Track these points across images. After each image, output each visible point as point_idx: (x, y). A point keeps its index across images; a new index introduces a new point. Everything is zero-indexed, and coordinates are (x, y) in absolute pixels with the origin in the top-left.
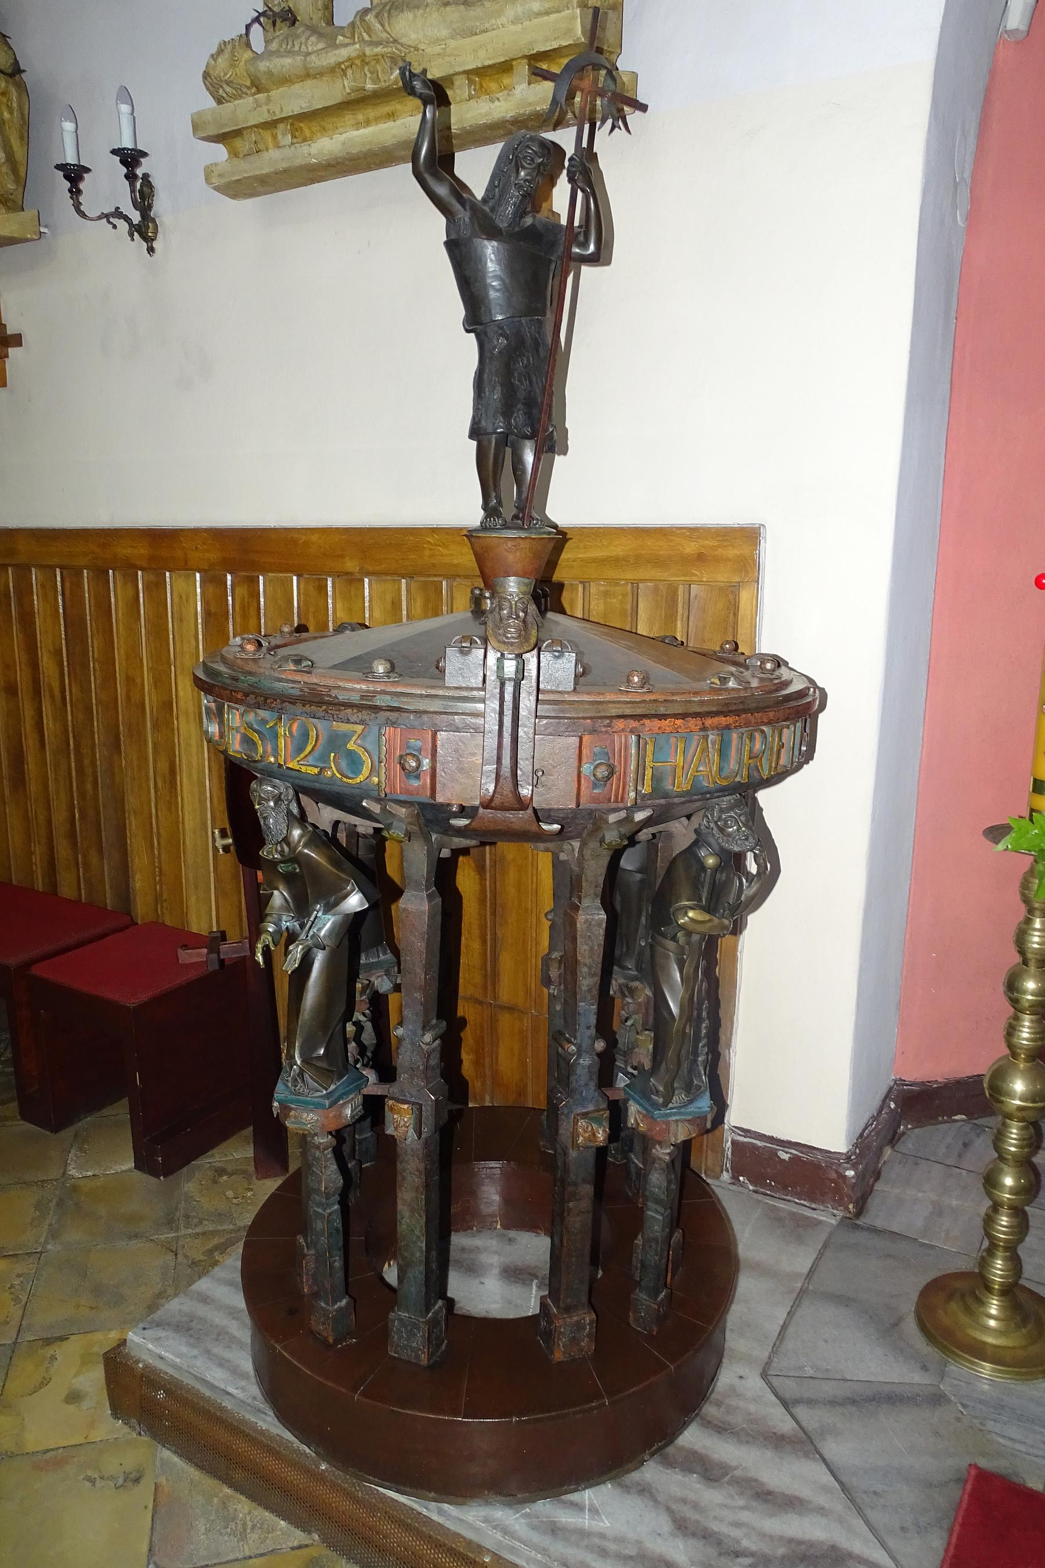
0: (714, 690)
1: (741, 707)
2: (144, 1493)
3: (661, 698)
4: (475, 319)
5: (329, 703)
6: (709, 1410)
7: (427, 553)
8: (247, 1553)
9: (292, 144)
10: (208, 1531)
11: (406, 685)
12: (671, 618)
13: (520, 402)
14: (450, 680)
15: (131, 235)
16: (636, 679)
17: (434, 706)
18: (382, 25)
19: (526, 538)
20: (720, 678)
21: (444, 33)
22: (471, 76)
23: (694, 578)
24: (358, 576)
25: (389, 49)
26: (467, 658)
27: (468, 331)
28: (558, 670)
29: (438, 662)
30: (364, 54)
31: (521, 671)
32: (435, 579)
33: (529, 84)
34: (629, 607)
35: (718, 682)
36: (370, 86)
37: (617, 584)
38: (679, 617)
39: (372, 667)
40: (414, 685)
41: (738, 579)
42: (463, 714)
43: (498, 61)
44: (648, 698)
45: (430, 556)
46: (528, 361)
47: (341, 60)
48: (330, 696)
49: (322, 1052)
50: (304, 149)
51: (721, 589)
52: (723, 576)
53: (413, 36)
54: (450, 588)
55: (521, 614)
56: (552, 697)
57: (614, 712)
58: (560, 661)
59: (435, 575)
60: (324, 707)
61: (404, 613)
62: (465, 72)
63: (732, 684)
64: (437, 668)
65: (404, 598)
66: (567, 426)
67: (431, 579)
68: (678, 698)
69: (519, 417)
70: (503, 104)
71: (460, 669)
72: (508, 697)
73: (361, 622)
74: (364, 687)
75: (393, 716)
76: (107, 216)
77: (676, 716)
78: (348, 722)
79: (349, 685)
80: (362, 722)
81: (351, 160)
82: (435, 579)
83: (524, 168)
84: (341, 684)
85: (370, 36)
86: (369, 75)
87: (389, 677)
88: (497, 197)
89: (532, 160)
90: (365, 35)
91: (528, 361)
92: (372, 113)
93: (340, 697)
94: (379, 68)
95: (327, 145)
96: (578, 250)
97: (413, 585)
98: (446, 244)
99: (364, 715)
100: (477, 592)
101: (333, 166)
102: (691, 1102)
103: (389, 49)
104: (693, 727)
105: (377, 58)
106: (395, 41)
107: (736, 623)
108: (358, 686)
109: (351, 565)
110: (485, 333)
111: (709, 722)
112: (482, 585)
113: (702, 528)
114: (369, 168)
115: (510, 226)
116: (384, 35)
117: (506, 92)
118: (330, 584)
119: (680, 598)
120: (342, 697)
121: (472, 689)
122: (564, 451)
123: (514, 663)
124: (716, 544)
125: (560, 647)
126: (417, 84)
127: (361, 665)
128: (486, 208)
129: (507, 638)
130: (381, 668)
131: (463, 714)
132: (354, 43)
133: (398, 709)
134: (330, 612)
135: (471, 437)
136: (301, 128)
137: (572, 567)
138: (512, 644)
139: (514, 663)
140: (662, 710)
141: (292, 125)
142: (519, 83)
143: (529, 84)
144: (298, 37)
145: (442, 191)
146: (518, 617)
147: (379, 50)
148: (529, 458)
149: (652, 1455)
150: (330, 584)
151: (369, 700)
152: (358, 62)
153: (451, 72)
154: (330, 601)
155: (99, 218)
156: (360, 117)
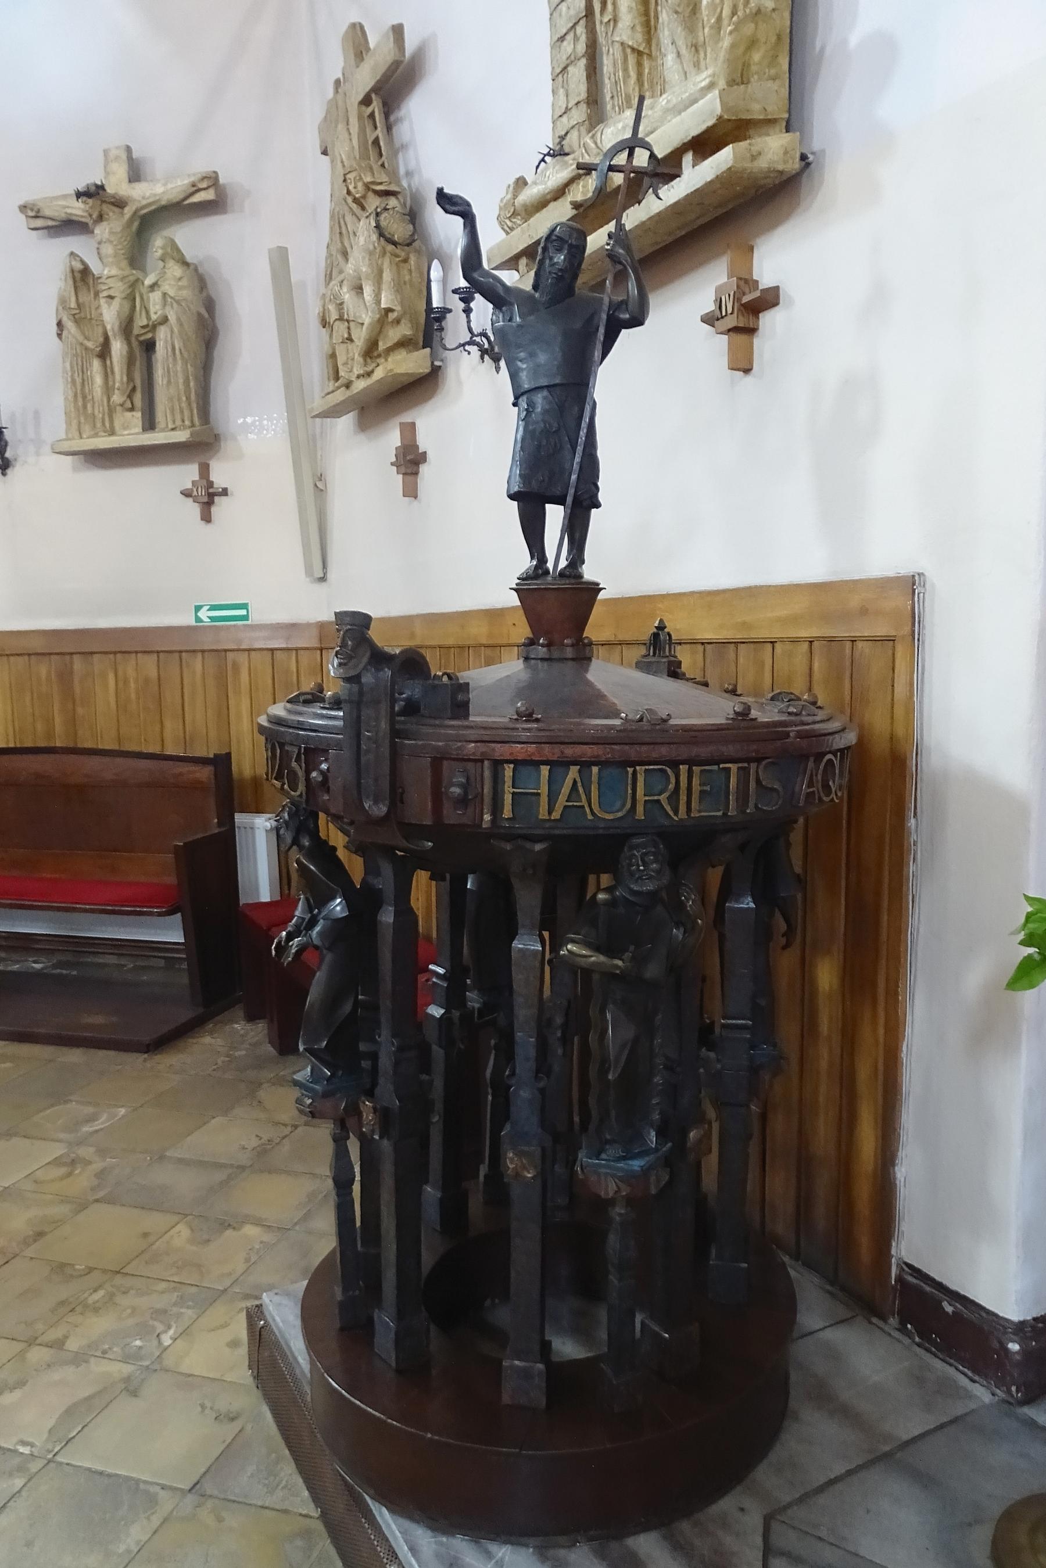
2: (229, 1431)
6: (685, 1526)
8: (267, 1505)
10: (252, 1476)
15: (482, 358)
49: (692, 1134)
66: (599, 484)
76: (463, 345)
102: (624, 1158)
149: (590, 1539)
155: (457, 348)
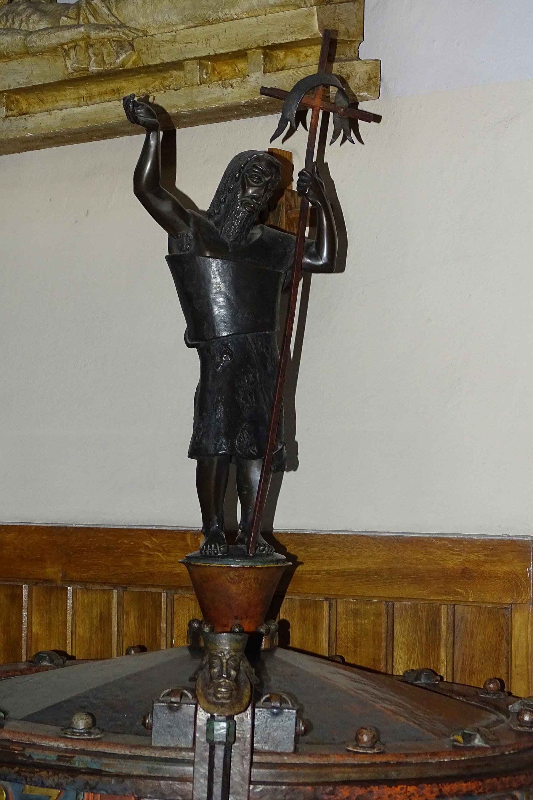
0: (457, 749)
1: (486, 770)
3: (392, 760)
4: (199, 331)
5: (23, 764)
7: (144, 559)
9: (7, 117)
11: (109, 744)
12: (432, 645)
13: (246, 414)
14: (158, 740)
16: (365, 738)
17: (139, 769)
18: (109, 10)
19: (250, 567)
20: (464, 736)
21: (175, 18)
22: (203, 61)
23: (458, 598)
24: (59, 583)
25: (116, 34)
26: (176, 714)
27: (189, 346)
28: (274, 728)
29: (145, 719)
30: (89, 37)
31: (232, 734)
32: (154, 590)
33: (265, 72)
34: (383, 630)
35: (460, 739)
36: (94, 68)
37: (369, 602)
38: (443, 642)
39: (72, 723)
40: (116, 744)
41: (509, 600)
42: (171, 778)
43: (232, 50)
44: (378, 760)
45: (149, 563)
46: (255, 377)
47: (62, 41)
48: (24, 755)
50: (20, 122)
51: (490, 611)
52: (493, 596)
53: (142, 21)
54: (171, 603)
55: (233, 673)
56: (269, 759)
57: (338, 776)
58: (279, 719)
59: (153, 586)
60: (17, 769)
61: (115, 629)
62: (195, 58)
63: (478, 741)
64: (144, 723)
65: (114, 611)
66: (297, 438)
67: (148, 590)
68: (413, 760)
69: (244, 436)
70: (236, 90)
71: (169, 726)
72: (219, 763)
73: (62, 649)
74: (62, 745)
75: (93, 780)
77: (408, 782)
78: (43, 785)
79: (45, 743)
80: (58, 786)
81: (69, 134)
82: (154, 590)
83: (250, 186)
84: (36, 741)
85: (96, 19)
86: (93, 58)
87: (90, 734)
88: (222, 211)
89: (260, 179)
90: (90, 17)
91: (255, 377)
92: (95, 89)
93: (35, 757)
94: (105, 51)
95: (44, 120)
96: (309, 261)
97: (126, 597)
98: (169, 259)
99: (61, 778)
100: (196, 625)
101: (49, 138)
103: (116, 34)
104: (428, 795)
105: (102, 42)
106: (123, 25)
107: (510, 652)
108: (54, 744)
109: (52, 571)
110: (208, 350)
111: (447, 788)
112: (200, 617)
113: (466, 540)
114: (90, 139)
115: (236, 240)
116: (112, 19)
117: (239, 79)
118: (25, 592)
119: (444, 620)
120: (37, 756)
121: (181, 749)
122: (294, 466)
123: (224, 725)
124: (483, 558)
125: (279, 701)
126: (141, 113)
127: (57, 715)
128: (211, 222)
129: (218, 698)
130: (81, 723)
131: (171, 778)
132: (79, 26)
133: (98, 773)
134: (24, 627)
135: (191, 455)
136: (17, 100)
137: (316, 581)
138: (223, 705)
139: (224, 725)
140: (393, 774)
141: (8, 97)
142: (253, 71)
143: (265, 72)
144: (19, 14)
145: (166, 207)
146: (229, 676)
147: (105, 33)
148: (256, 475)
150: (25, 592)
151: (67, 762)
152: (82, 44)
153: (181, 58)
154: (25, 614)
156: (83, 92)
